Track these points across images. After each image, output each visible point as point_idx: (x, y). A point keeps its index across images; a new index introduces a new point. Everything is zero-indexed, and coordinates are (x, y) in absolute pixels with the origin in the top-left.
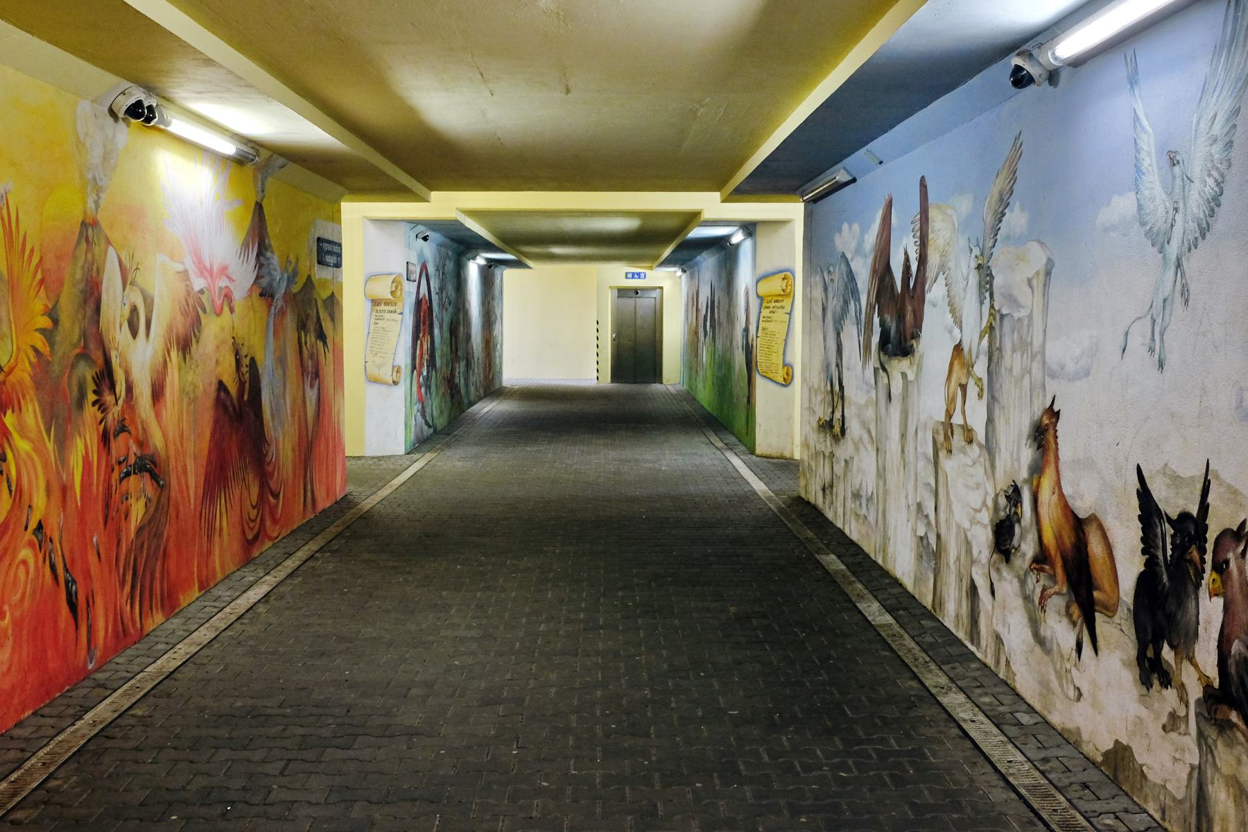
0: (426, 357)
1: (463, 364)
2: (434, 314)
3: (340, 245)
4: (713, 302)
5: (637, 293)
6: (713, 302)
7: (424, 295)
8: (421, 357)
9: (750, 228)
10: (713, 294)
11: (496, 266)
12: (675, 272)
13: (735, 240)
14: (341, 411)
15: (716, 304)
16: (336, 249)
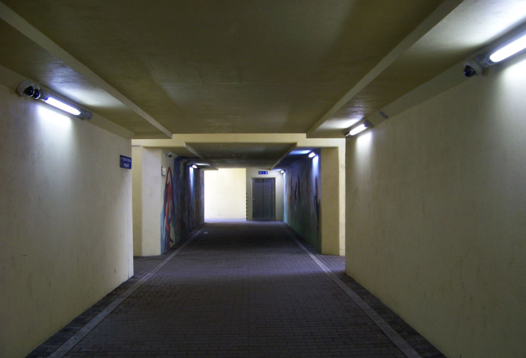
0: (170, 210)
1: (187, 213)
2: (174, 191)
3: (131, 159)
4: (299, 184)
5: (264, 180)
6: (299, 184)
7: (169, 182)
8: (168, 211)
9: (317, 150)
10: (299, 180)
11: (201, 169)
12: (281, 171)
13: (311, 156)
14: (163, 216)
15: (301, 185)
16: (129, 161)
